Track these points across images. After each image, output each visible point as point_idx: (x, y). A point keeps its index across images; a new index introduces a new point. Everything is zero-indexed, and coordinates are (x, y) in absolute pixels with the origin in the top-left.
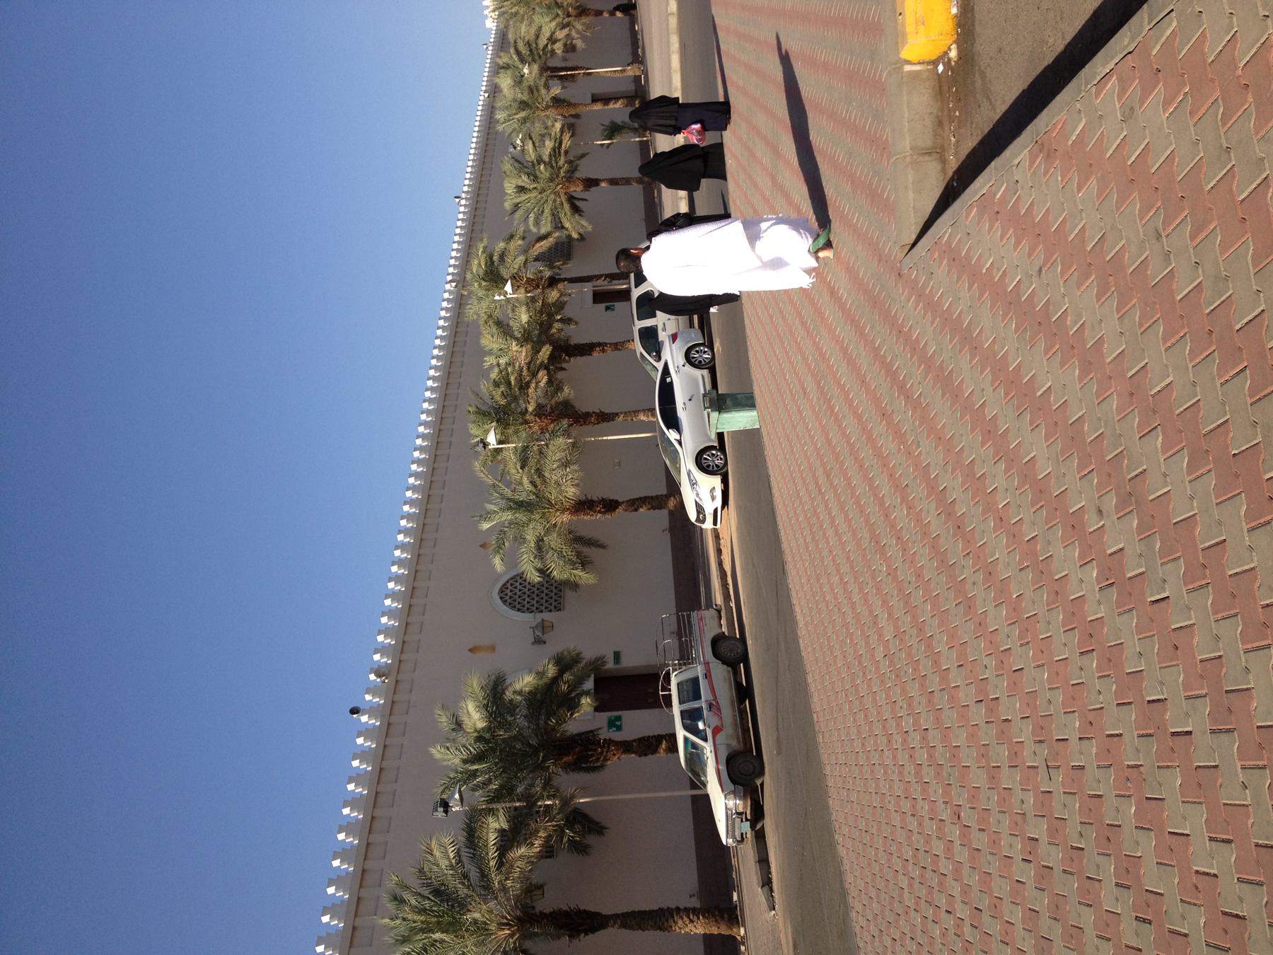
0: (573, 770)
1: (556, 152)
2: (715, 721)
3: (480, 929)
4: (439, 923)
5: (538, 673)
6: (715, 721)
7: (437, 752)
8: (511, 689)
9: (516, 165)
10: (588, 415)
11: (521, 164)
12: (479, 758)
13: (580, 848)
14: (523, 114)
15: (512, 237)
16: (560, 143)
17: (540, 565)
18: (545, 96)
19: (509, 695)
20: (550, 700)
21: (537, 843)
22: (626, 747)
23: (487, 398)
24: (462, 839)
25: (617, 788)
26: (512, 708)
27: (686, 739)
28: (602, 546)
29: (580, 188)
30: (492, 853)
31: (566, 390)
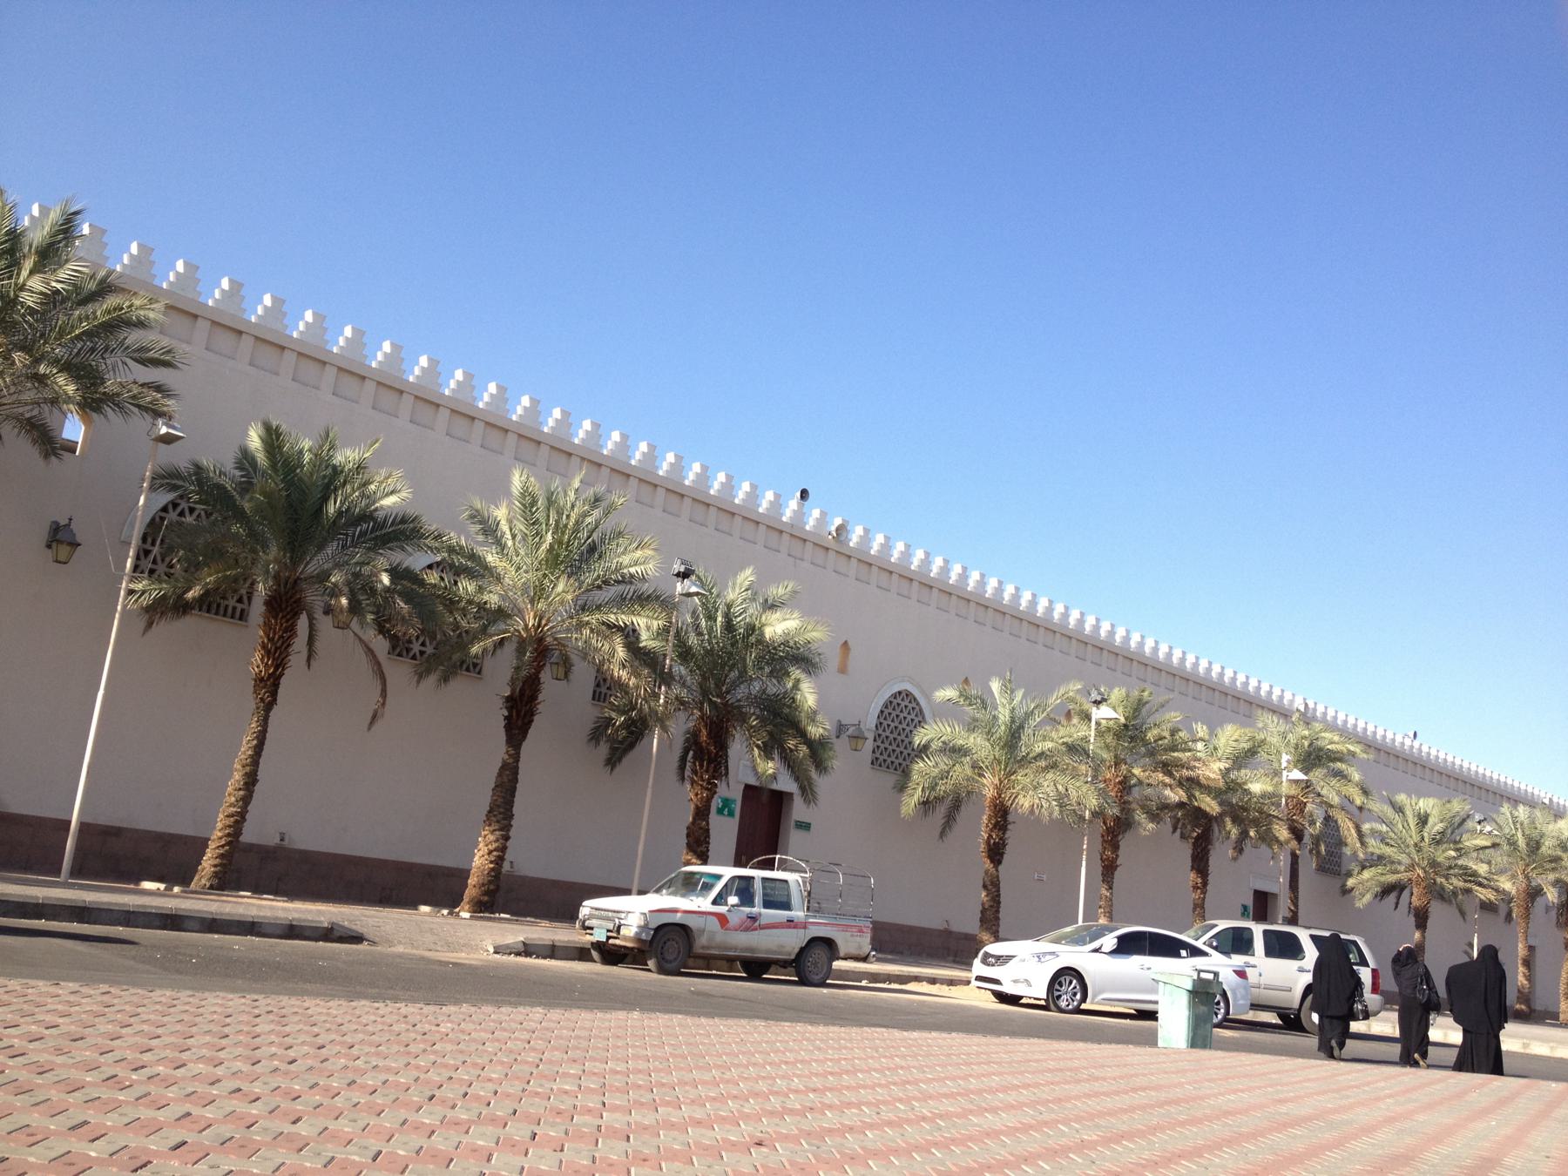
0: (687, 740)
1: (1470, 875)
2: (734, 920)
3: (539, 592)
4: (560, 543)
5: (815, 712)
6: (734, 920)
7: (746, 576)
8: (803, 676)
9: (1457, 820)
10: (1115, 847)
11: (1452, 833)
12: (729, 626)
13: (596, 735)
14: (1522, 842)
15: (1365, 792)
16: (1480, 885)
17: (934, 746)
18: (1545, 881)
19: (796, 673)
20: (781, 722)
21: (624, 674)
22: (702, 813)
23: (1157, 718)
24: (646, 588)
25: (657, 786)
26: (780, 674)
27: (719, 877)
28: (942, 834)
29: (1416, 902)
30: (623, 619)
31: (1150, 826)
